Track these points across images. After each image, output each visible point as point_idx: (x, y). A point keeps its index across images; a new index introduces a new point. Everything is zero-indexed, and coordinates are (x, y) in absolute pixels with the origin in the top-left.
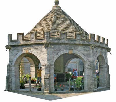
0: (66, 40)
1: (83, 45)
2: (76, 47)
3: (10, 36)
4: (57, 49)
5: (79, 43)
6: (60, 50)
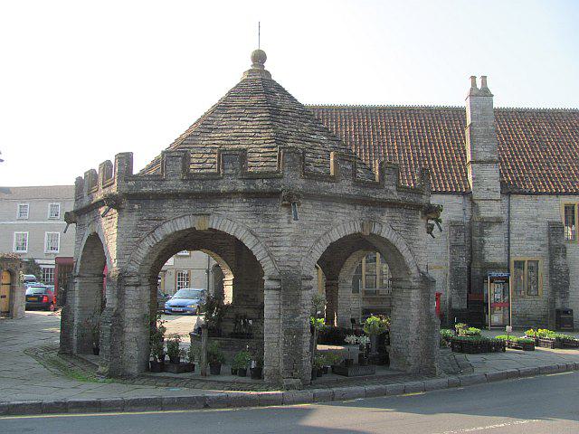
0: (182, 180)
1: (247, 194)
2: (224, 205)
3: (473, 78)
4: (152, 215)
5: (232, 188)
6: (161, 221)
